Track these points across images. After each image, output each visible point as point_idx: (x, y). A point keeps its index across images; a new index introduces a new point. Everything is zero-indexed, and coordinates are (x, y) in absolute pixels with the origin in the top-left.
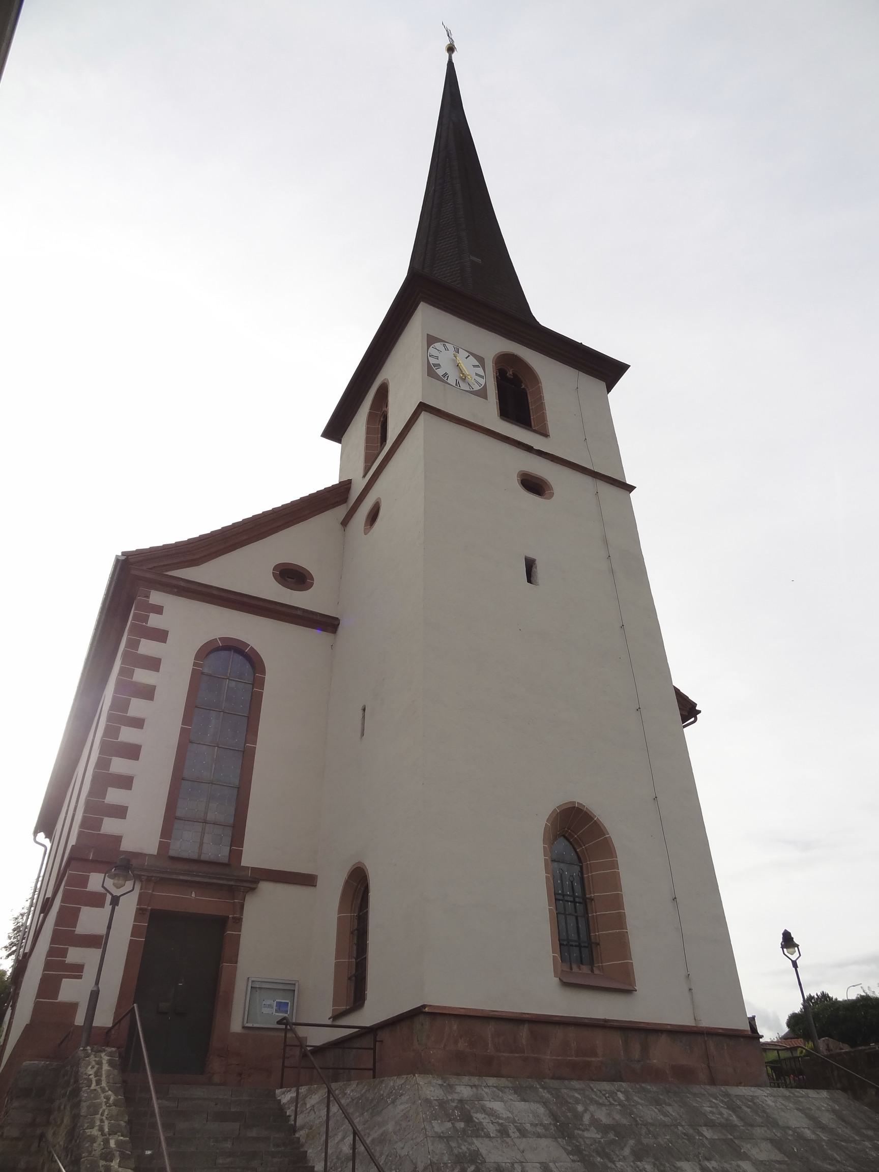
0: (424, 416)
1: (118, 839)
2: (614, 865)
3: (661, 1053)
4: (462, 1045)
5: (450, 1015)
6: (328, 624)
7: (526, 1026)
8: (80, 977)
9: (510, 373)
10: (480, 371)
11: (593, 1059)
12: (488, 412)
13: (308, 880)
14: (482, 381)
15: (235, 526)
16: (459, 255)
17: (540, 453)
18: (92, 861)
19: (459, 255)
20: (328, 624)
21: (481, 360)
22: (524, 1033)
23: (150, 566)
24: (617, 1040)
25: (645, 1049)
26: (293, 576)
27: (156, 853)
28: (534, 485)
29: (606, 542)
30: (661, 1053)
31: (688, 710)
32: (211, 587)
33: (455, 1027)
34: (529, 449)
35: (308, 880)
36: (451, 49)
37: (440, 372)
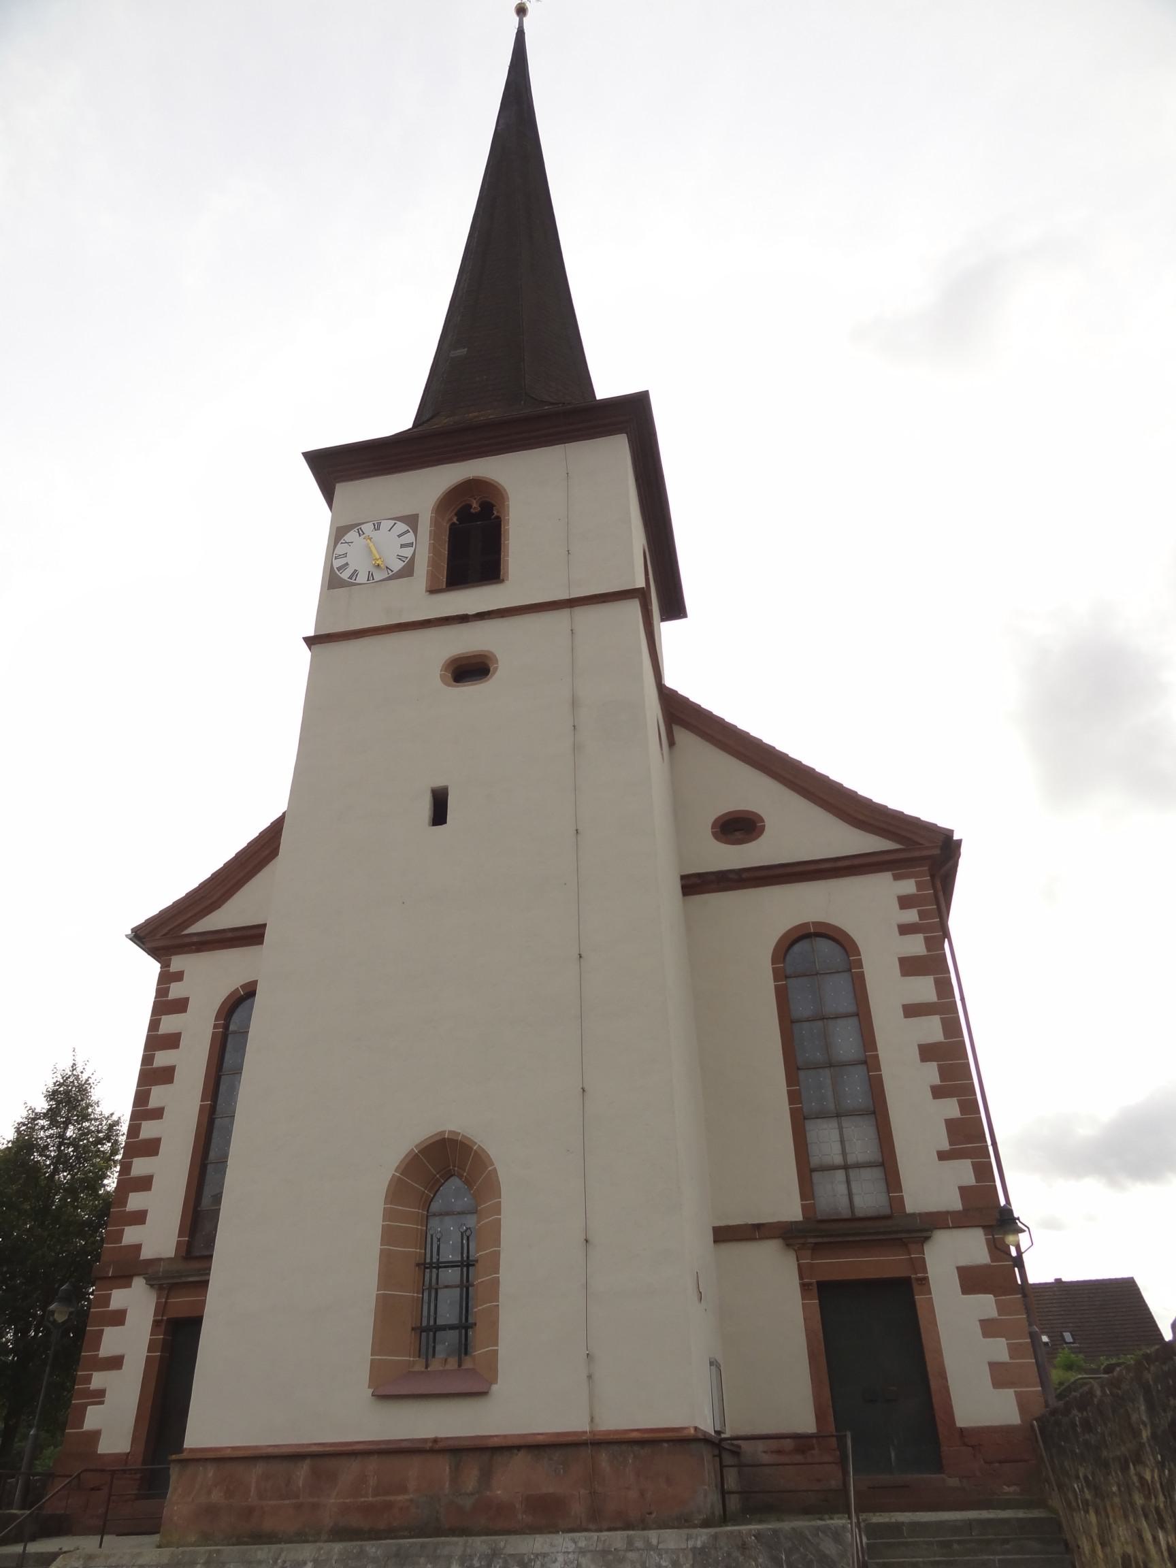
1: (138, 1248)
3: (510, 1482)
4: (217, 1496)
5: (206, 1459)
7: (308, 1461)
8: (102, 1403)
10: (410, 537)
11: (400, 1498)
15: (250, 845)
16: (510, 355)
17: (481, 616)
18: (112, 1277)
19: (510, 355)
21: (412, 521)
22: (302, 1472)
23: (165, 931)
24: (443, 1466)
25: (486, 1476)
27: (172, 1255)
28: (470, 670)
29: (574, 703)
30: (510, 1482)
31: (924, 858)
32: (224, 931)
33: (210, 1475)
34: (463, 619)
36: (521, 11)
37: (345, 575)
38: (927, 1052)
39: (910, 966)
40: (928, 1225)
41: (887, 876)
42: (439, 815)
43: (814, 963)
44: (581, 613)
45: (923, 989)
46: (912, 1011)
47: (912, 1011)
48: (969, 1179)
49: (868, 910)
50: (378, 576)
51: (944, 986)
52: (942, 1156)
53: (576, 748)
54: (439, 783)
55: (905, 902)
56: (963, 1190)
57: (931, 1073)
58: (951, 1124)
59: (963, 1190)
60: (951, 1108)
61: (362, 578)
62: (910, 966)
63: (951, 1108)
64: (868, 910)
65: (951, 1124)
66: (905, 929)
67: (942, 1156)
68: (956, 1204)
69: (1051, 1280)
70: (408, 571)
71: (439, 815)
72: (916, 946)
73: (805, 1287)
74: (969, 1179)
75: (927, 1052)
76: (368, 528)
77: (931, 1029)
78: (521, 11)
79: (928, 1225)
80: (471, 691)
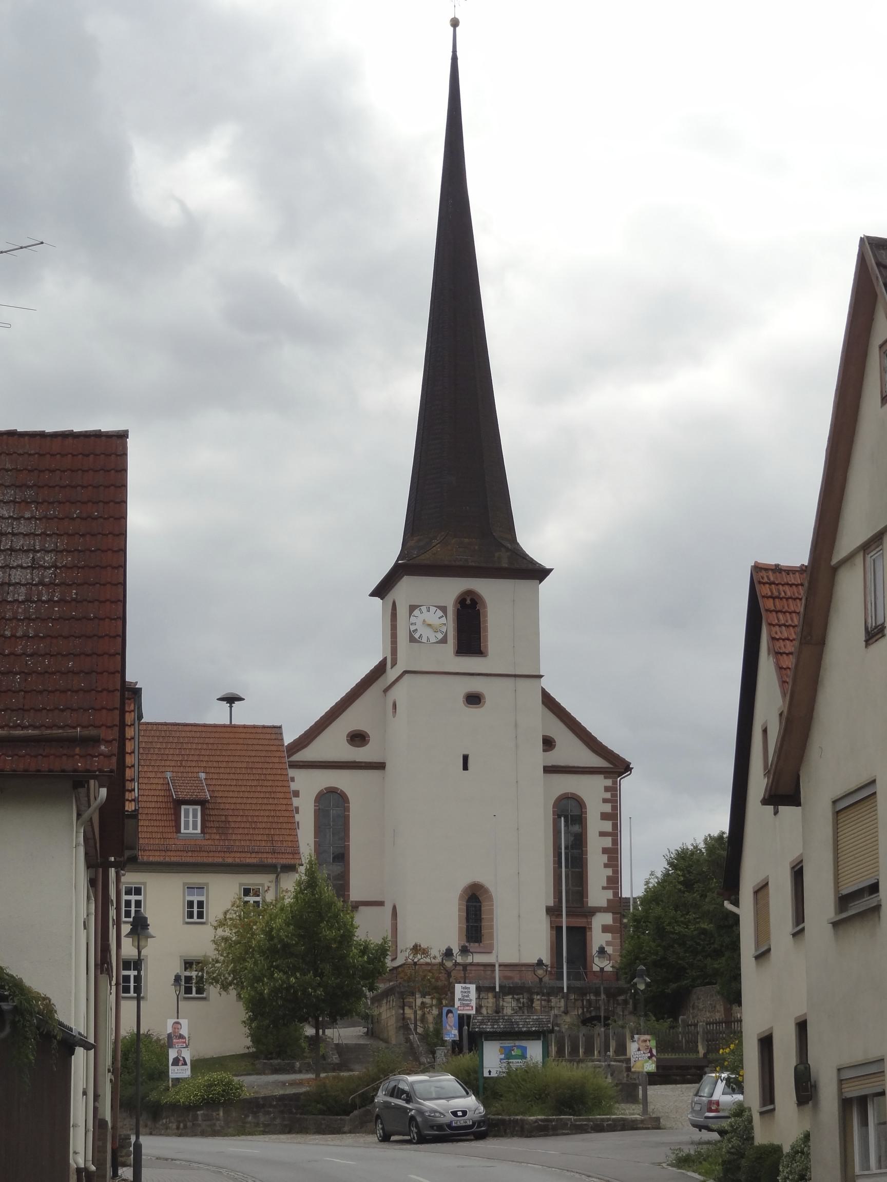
2: (492, 905)
6: (380, 766)
9: (468, 602)
10: (444, 620)
13: (380, 904)
20: (380, 766)
21: (444, 609)
26: (358, 738)
28: (474, 699)
31: (618, 767)
35: (380, 904)
36: (455, 23)
37: (417, 636)
38: (605, 851)
39: (604, 816)
40: (594, 911)
41: (602, 776)
42: (466, 758)
43: (569, 812)
44: (521, 682)
45: (607, 826)
46: (602, 834)
47: (602, 834)
48: (611, 897)
49: (591, 790)
50: (433, 640)
51: (615, 826)
52: (604, 888)
53: (517, 746)
54: (466, 753)
55: (607, 789)
56: (608, 900)
57: (605, 859)
58: (608, 877)
59: (608, 900)
60: (609, 872)
61: (424, 640)
62: (604, 816)
63: (609, 872)
64: (591, 790)
65: (608, 877)
66: (605, 801)
67: (604, 888)
68: (605, 904)
69: (799, 565)
70: (444, 641)
71: (466, 758)
72: (608, 808)
73: (552, 927)
74: (611, 897)
75: (605, 851)
76: (424, 609)
77: (608, 842)
78: (455, 23)
79: (594, 911)
80: (473, 711)
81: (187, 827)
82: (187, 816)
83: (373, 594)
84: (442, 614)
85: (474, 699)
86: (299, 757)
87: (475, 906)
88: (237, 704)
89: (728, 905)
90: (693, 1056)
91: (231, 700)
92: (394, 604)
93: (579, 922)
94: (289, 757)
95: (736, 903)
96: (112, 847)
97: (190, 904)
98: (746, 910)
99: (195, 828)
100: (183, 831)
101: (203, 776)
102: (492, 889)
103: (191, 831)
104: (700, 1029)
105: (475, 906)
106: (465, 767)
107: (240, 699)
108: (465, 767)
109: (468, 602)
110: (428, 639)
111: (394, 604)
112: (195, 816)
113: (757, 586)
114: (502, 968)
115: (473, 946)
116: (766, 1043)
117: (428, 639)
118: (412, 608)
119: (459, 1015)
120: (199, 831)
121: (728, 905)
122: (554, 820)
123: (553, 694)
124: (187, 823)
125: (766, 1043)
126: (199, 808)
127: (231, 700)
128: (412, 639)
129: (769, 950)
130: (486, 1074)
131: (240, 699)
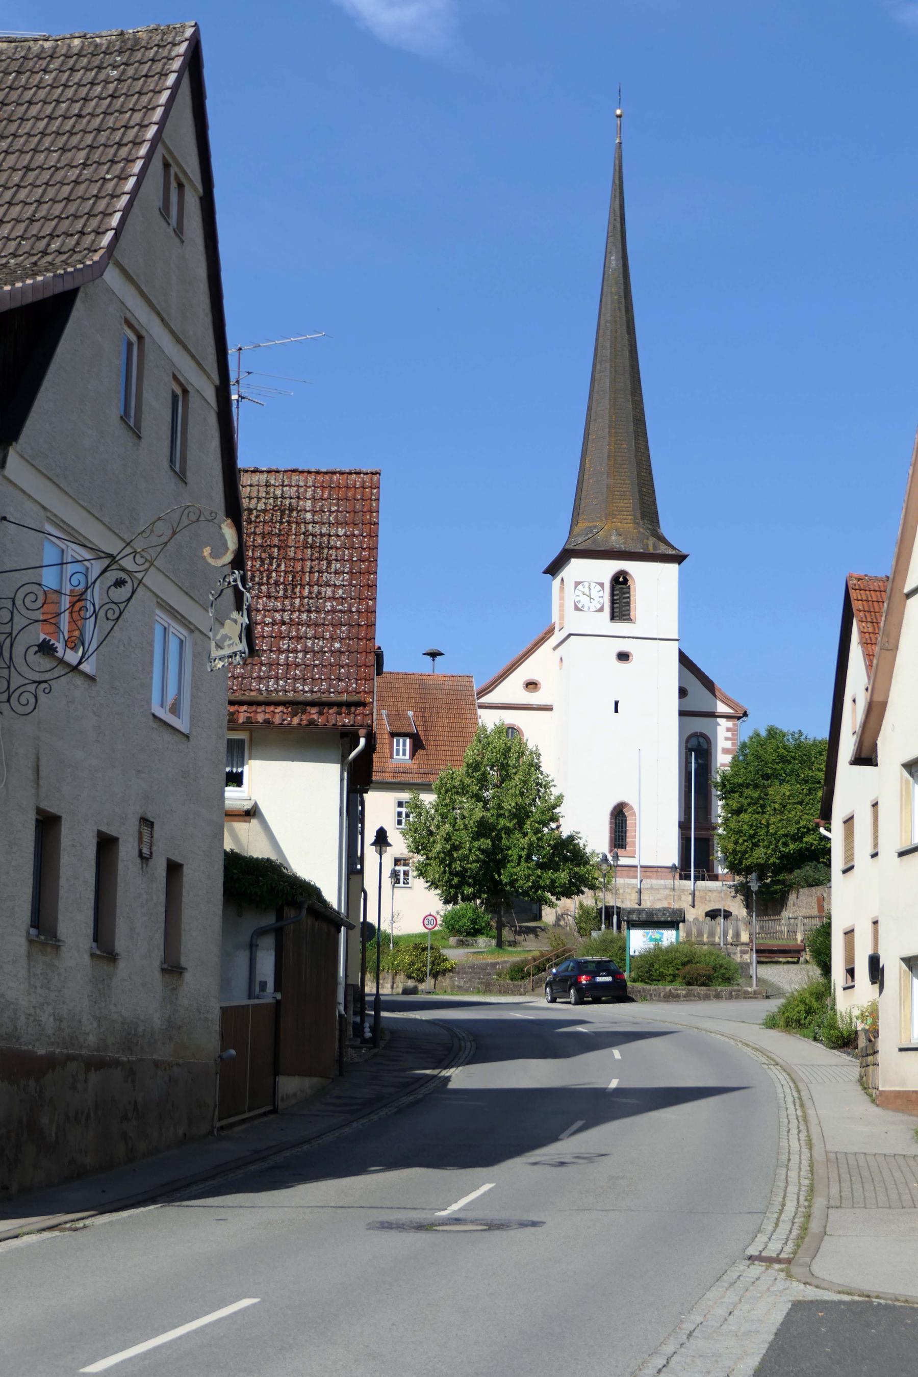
0: (831, 1211)
9: (621, 579)
10: (601, 594)
12: (603, 622)
14: (601, 600)
26: (532, 685)
28: (623, 656)
37: (580, 606)
42: (617, 703)
70: (601, 610)
81: (398, 754)
82: (398, 745)
83: (545, 572)
84: (600, 588)
85: (623, 656)
86: (485, 700)
87: (619, 817)
88: (438, 658)
89: (822, 830)
90: (792, 943)
91: (434, 655)
92: (562, 580)
93: (703, 834)
94: (478, 699)
95: (829, 830)
96: (359, 780)
97: (400, 814)
98: (836, 835)
99: (404, 754)
100: (395, 757)
101: (410, 713)
102: (636, 808)
103: (401, 756)
104: (799, 922)
105: (619, 817)
106: (617, 703)
107: (441, 654)
108: (616, 711)
109: (621, 579)
110: (589, 608)
111: (562, 580)
112: (404, 745)
113: (852, 592)
114: (643, 869)
115: (620, 852)
116: (849, 933)
117: (589, 608)
118: (577, 584)
119: (228, 740)
120: (407, 757)
121: (822, 830)
122: (686, 753)
123: (687, 654)
124: (398, 751)
125: (849, 933)
126: (408, 741)
127: (434, 655)
128: (577, 608)
129: (852, 867)
130: (632, 953)
131: (441, 654)
